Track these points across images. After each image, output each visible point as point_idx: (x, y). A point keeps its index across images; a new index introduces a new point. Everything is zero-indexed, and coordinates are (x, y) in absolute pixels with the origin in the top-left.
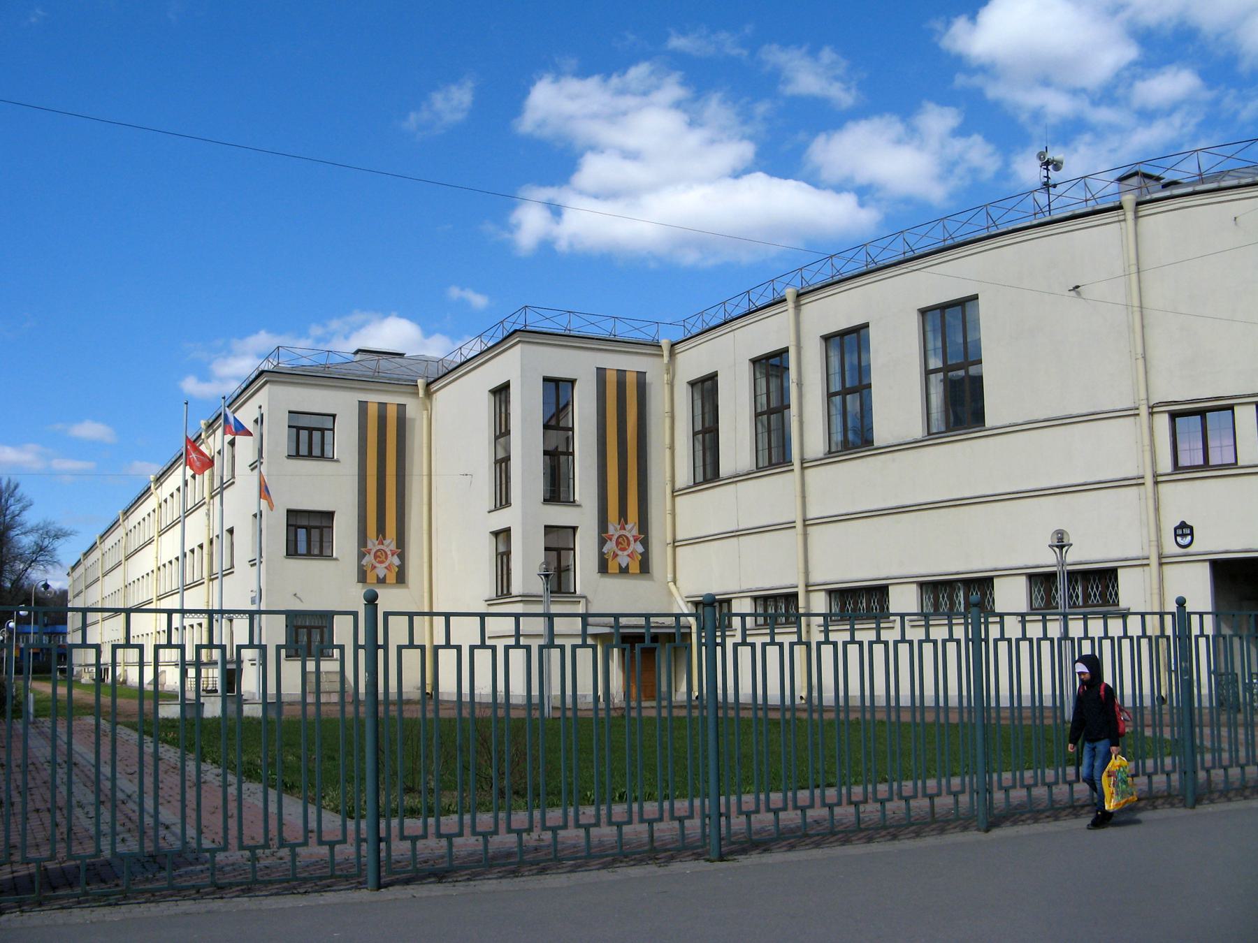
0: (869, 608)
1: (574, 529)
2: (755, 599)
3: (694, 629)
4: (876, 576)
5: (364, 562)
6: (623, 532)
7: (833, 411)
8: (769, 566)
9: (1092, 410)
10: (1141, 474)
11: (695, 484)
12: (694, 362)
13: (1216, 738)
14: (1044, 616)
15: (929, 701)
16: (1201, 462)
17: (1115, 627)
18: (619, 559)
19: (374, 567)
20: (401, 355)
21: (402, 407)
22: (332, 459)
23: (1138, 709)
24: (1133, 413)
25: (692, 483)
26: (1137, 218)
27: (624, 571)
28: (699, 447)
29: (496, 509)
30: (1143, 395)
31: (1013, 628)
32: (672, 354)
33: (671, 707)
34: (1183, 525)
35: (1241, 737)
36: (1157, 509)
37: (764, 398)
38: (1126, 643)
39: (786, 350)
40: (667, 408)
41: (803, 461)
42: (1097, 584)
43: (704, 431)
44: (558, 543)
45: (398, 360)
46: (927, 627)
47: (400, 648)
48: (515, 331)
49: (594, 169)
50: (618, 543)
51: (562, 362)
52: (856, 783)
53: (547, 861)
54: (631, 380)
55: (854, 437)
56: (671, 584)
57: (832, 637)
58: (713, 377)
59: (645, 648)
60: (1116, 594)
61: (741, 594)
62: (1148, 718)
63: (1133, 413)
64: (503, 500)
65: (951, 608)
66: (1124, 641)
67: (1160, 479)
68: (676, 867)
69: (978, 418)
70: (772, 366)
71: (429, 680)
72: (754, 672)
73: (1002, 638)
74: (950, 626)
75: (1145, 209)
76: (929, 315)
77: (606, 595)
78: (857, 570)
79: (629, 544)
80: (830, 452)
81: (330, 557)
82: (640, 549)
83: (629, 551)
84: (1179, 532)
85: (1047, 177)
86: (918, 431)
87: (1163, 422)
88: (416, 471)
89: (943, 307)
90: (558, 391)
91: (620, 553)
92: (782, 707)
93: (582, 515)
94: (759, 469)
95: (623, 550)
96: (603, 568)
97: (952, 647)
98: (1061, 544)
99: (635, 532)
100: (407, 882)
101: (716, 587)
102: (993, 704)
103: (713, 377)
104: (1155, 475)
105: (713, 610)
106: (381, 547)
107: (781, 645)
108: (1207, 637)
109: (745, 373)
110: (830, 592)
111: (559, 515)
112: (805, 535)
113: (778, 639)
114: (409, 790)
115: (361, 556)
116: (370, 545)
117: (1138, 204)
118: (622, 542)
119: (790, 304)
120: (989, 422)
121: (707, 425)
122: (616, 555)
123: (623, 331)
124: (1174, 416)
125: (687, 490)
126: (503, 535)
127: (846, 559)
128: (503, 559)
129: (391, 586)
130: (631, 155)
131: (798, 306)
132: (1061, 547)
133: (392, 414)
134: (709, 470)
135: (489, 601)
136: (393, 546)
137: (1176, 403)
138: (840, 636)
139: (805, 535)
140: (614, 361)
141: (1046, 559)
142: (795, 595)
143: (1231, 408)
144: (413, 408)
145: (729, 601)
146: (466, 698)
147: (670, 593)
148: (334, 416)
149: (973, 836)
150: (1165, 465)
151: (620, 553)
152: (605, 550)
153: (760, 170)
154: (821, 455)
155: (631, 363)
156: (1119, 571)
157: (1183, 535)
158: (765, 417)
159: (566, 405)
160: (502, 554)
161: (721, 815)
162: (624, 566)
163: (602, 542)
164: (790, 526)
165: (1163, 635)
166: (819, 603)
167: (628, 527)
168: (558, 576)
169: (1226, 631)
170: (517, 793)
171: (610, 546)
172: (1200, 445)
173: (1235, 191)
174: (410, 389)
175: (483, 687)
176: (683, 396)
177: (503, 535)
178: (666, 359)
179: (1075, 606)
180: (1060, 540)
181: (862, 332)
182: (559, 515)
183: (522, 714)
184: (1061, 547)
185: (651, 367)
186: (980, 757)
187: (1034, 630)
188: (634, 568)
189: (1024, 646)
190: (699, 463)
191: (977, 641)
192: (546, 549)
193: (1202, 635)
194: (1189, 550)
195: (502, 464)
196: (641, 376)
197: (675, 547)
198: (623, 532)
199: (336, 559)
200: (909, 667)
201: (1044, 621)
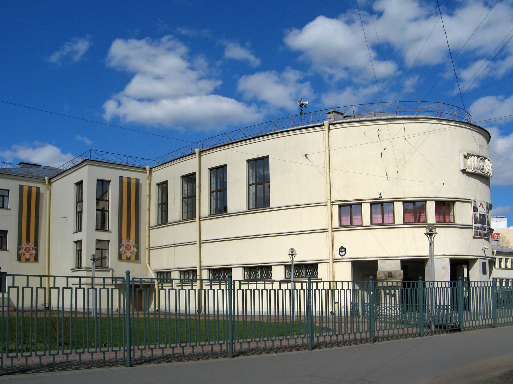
0: (262, 275)
1: (108, 241)
2: (180, 272)
3: (156, 283)
4: (227, 264)
5: (20, 252)
6: (129, 243)
7: (212, 198)
8: (187, 259)
9: (310, 203)
10: (327, 228)
11: (158, 225)
12: (160, 175)
14: (265, 282)
15: (249, 313)
16: (380, 221)
17: (269, 286)
18: (126, 254)
20: (40, 166)
21: (38, 188)
22: (7, 209)
23: (321, 317)
25: (157, 225)
26: (329, 130)
27: (28, 260)
28: (160, 210)
29: (76, 232)
30: (329, 198)
31: (276, 286)
32: (150, 172)
33: (149, 314)
35: (349, 326)
36: (332, 241)
37: (186, 192)
38: (280, 292)
39: (194, 174)
40: (148, 194)
41: (200, 217)
42: (309, 269)
43: (162, 204)
44: (102, 246)
45: (38, 169)
46: (211, 285)
48: (86, 160)
49: (137, 86)
50: (126, 248)
51: (105, 173)
53: (64, 366)
54: (133, 182)
55: (220, 208)
56: (148, 265)
58: (166, 182)
59: (138, 291)
60: (317, 273)
61: (175, 270)
62: (324, 320)
63: (324, 204)
64: (79, 229)
65: (256, 277)
66: (91, 290)
67: (334, 230)
68: (114, 368)
70: (189, 179)
71: (47, 302)
72: (171, 300)
73: (317, 289)
74: (220, 285)
75: (332, 127)
76: (250, 163)
77: (118, 268)
78: (221, 262)
79: (131, 248)
80: (211, 214)
81: (5, 250)
82: (135, 250)
83: (30, 253)
84: (341, 250)
85: (302, 110)
86: (244, 208)
87: (336, 208)
88: (43, 215)
89: (256, 160)
90: (103, 185)
91: (127, 251)
92: (186, 314)
93: (111, 236)
94: (183, 220)
95: (128, 250)
96: (120, 257)
97: (220, 292)
98: (292, 254)
99: (134, 243)
100: (10, 374)
101: (164, 266)
102: (236, 314)
103: (166, 182)
104: (332, 228)
105: (164, 276)
106: (27, 246)
108: (350, 290)
110: (209, 270)
111: (102, 236)
112: (200, 247)
113: (184, 288)
114: (24, 343)
115: (19, 249)
116: (23, 245)
117: (330, 124)
118: (128, 247)
119: (197, 155)
120: (272, 205)
121: (164, 201)
122: (125, 253)
123: (131, 162)
124: (340, 206)
126: (79, 243)
127: (216, 257)
128: (79, 253)
129: (32, 262)
130: (158, 78)
131: (200, 156)
132: (292, 255)
133: (34, 190)
134: (163, 220)
135: (73, 270)
136: (33, 246)
137: (341, 201)
138: (244, 287)
139: (200, 247)
140: (127, 174)
141: (287, 259)
142: (196, 271)
144: (43, 189)
145: (170, 272)
146: (61, 309)
147: (147, 269)
148: (9, 191)
149: (228, 359)
150: (336, 224)
151: (127, 251)
152: (121, 250)
154: (207, 216)
155: (134, 175)
156: (318, 264)
157: (342, 252)
158: (186, 199)
159: (106, 192)
160: (78, 251)
161: (131, 350)
162: (128, 257)
163: (120, 247)
166: (205, 275)
167: (131, 241)
168: (100, 261)
169: (357, 287)
170: (66, 344)
171: (123, 249)
172: (350, 217)
173: (349, 124)
174: (42, 181)
175: (67, 305)
176: (154, 190)
177: (79, 243)
178: (148, 174)
179: (299, 277)
180: (292, 252)
181: (225, 167)
182: (102, 236)
183: (69, 315)
185: (142, 177)
188: (32, 259)
190: (160, 216)
191: (310, 289)
192: (96, 249)
193: (317, 289)
195: (79, 214)
196: (138, 180)
197: (149, 250)
198: (129, 243)
199: (8, 251)
200: (273, 299)
201: (265, 284)
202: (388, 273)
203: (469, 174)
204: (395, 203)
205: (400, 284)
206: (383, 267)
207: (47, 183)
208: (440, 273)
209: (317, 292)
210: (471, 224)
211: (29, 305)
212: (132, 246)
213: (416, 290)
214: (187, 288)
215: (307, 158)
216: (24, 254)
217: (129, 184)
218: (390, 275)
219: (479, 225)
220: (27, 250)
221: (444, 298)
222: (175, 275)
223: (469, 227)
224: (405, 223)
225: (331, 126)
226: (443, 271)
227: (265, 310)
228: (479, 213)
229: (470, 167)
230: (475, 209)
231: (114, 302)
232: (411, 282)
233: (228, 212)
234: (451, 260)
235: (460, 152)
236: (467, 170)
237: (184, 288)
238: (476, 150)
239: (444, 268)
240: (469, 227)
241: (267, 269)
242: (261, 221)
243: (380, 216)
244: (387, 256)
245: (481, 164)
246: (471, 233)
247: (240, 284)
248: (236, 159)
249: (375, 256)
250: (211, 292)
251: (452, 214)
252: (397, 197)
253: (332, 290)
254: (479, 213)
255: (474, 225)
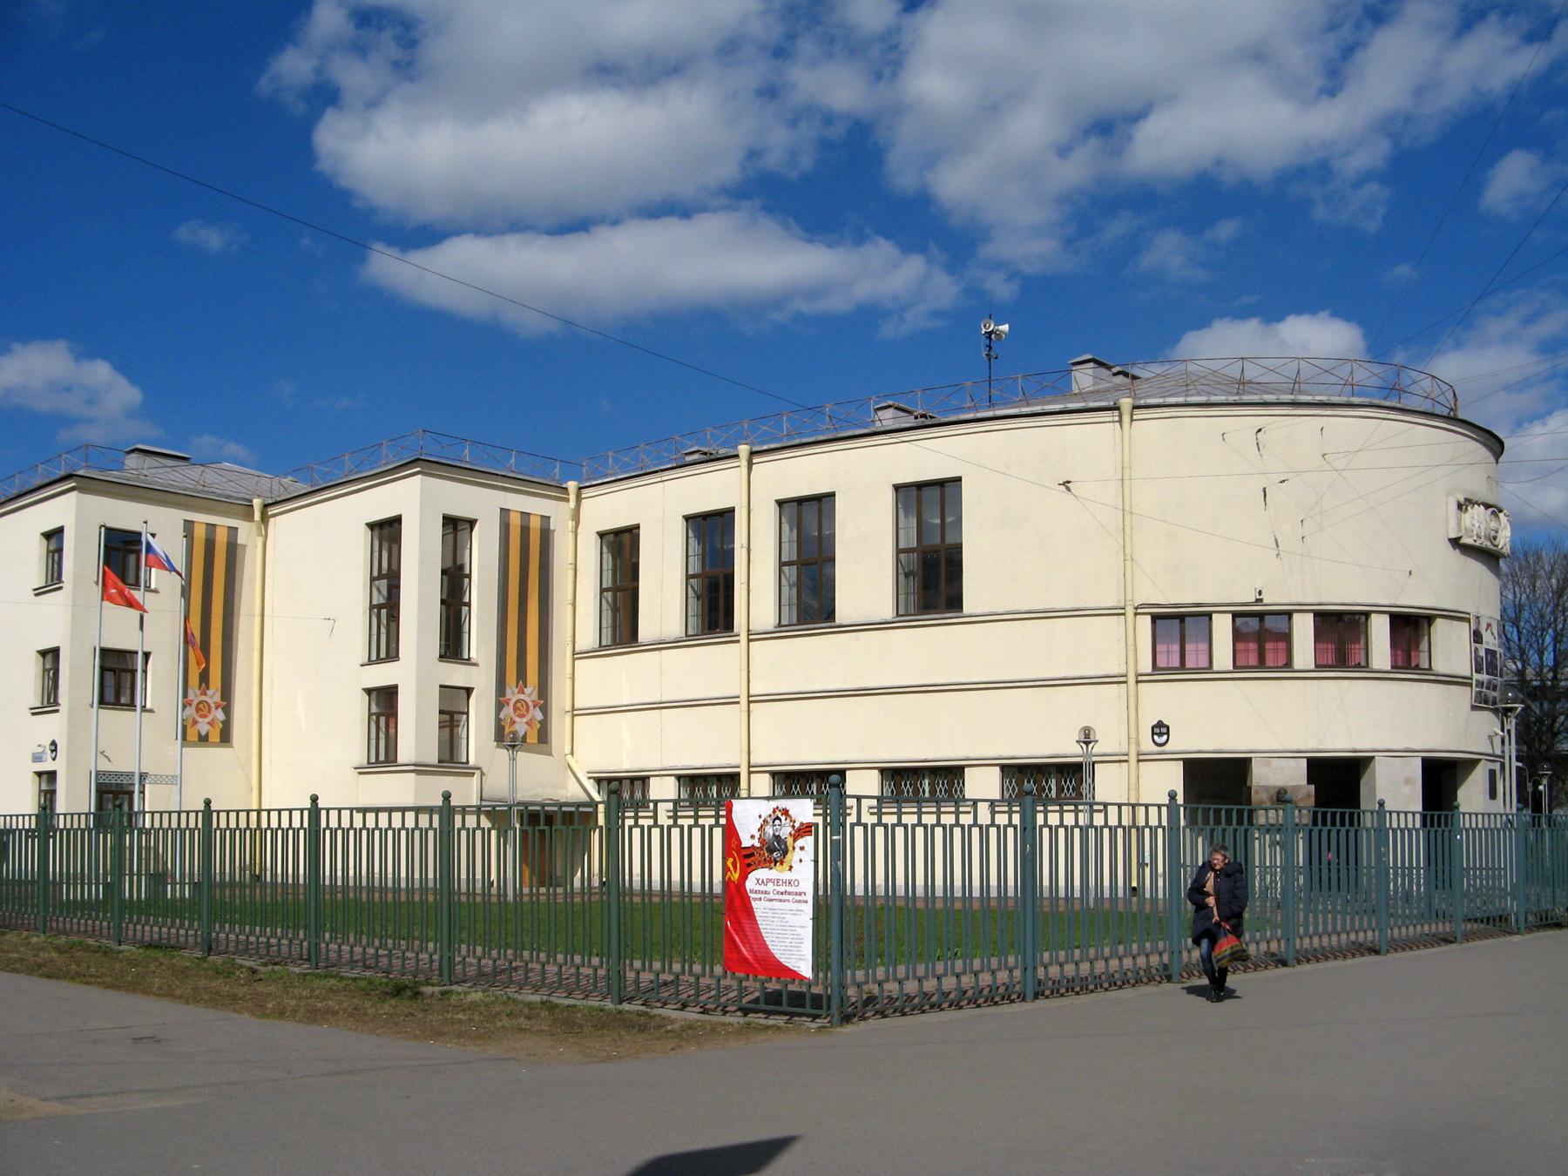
0: (933, 791)
1: (469, 691)
13: (1306, 919)
16: (1176, 663)
18: (198, 726)
19: (195, 722)
24: (1118, 612)
27: (203, 740)
29: (370, 662)
32: (579, 499)
34: (1160, 724)
40: (571, 559)
50: (198, 709)
52: (859, 968)
54: (535, 524)
57: (641, 822)
59: (546, 830)
61: (662, 773)
63: (1118, 612)
64: (386, 647)
69: (954, 603)
73: (859, 823)
80: (780, 625)
82: (539, 716)
86: (887, 611)
87: (1145, 623)
90: (456, 527)
93: (479, 673)
95: (522, 716)
97: (1010, 831)
101: (624, 762)
105: (624, 790)
107: (682, 827)
108: (1015, 827)
109: (676, 534)
111: (456, 675)
119: (744, 462)
120: (968, 607)
124: (1155, 618)
125: (588, 654)
129: (215, 745)
131: (750, 465)
132: (1087, 743)
133: (221, 537)
136: (217, 698)
142: (738, 774)
144: (246, 533)
145: (644, 780)
150: (1146, 665)
153: (1184, 331)
157: (1160, 735)
163: (500, 706)
164: (732, 701)
165: (1160, 825)
167: (210, 692)
171: (508, 712)
178: (572, 504)
180: (1087, 736)
182: (456, 675)
184: (1087, 743)
185: (557, 512)
186: (1029, 939)
187: (1002, 819)
188: (215, 737)
189: (993, 831)
193: (859, 823)
194: (1166, 748)
196: (546, 519)
198: (522, 697)
202: (1279, 793)
203: (1467, 550)
204: (1295, 616)
205: (1307, 820)
206: (1263, 777)
207: (257, 516)
208: (1395, 790)
210: (1468, 674)
213: (1246, 831)
214: (686, 822)
215: (1068, 489)
216: (513, 722)
217: (525, 530)
218: (1281, 797)
219: (1484, 677)
221: (1407, 852)
222: (663, 790)
223: (1463, 682)
224: (1319, 666)
225: (1136, 411)
226: (1406, 790)
227: (676, 877)
228: (1484, 646)
229: (1469, 532)
230: (1477, 637)
231: (491, 863)
233: (838, 620)
234: (1425, 761)
235: (1449, 493)
236: (1466, 540)
237: (701, 821)
238: (1481, 491)
239: (1408, 781)
240: (1463, 682)
241: (950, 775)
242: (932, 648)
243: (1176, 647)
244: (1281, 748)
245: (1493, 524)
246: (1464, 696)
247: (993, 813)
248: (862, 480)
249: (1243, 748)
250: (696, 832)
251: (1424, 646)
252: (1301, 601)
253: (1066, 828)
254: (1484, 646)
255: (1476, 676)
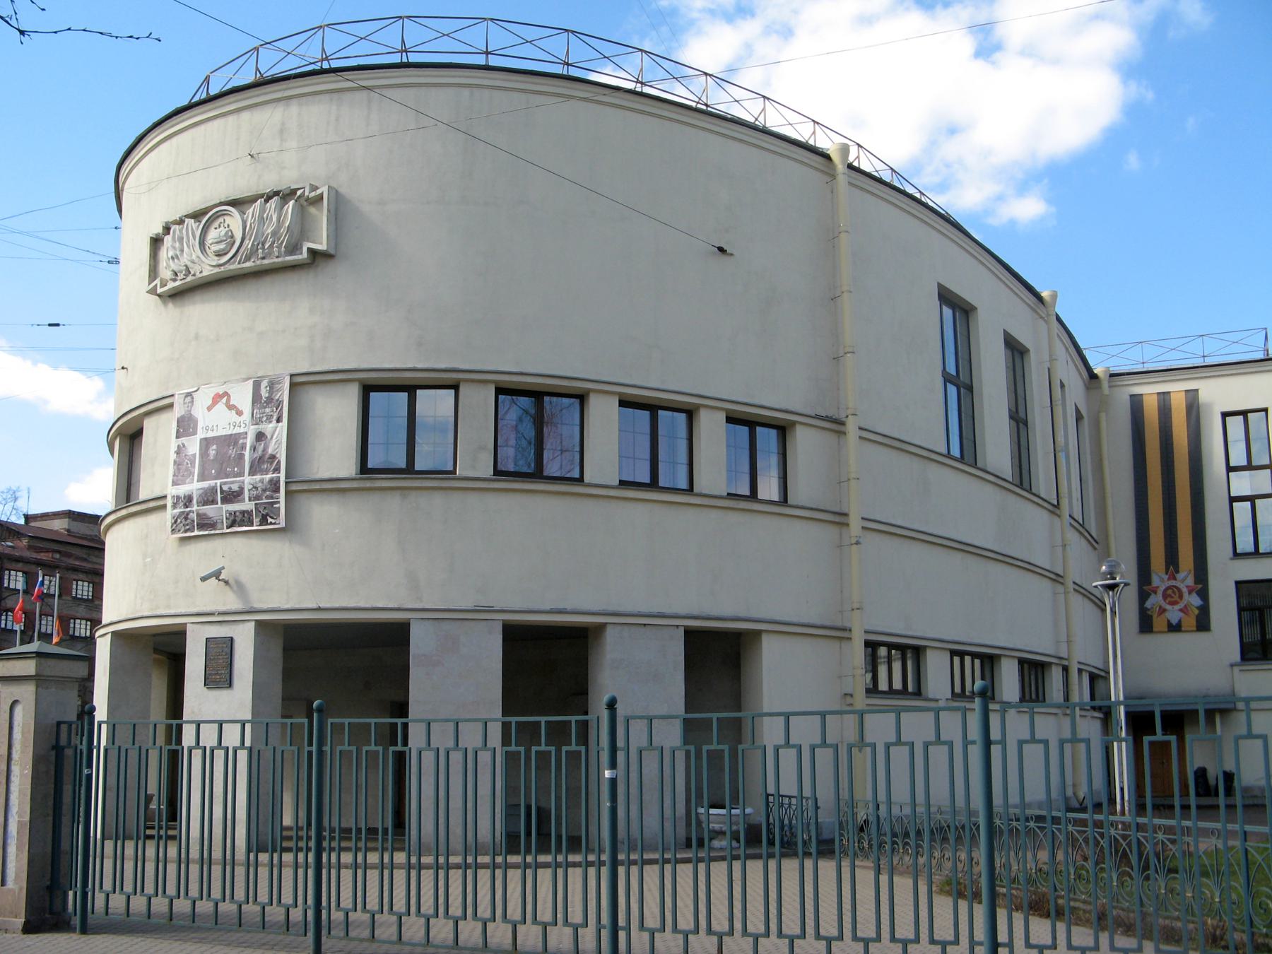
19: (1162, 611)
27: (1175, 628)
47: (1021, 743)
79: (1181, 597)
83: (1181, 605)
95: (1173, 603)
99: (1190, 581)
106: (1172, 583)
116: (1155, 581)
124: (368, 389)
143: (624, 484)
148: (1266, 410)
151: (1168, 607)
163: (1143, 596)
167: (1180, 576)
171: (1154, 601)
173: (1022, 288)
209: (197, 755)
211: (1042, 796)
212: (1185, 590)
220: (1172, 595)
232: (573, 719)
